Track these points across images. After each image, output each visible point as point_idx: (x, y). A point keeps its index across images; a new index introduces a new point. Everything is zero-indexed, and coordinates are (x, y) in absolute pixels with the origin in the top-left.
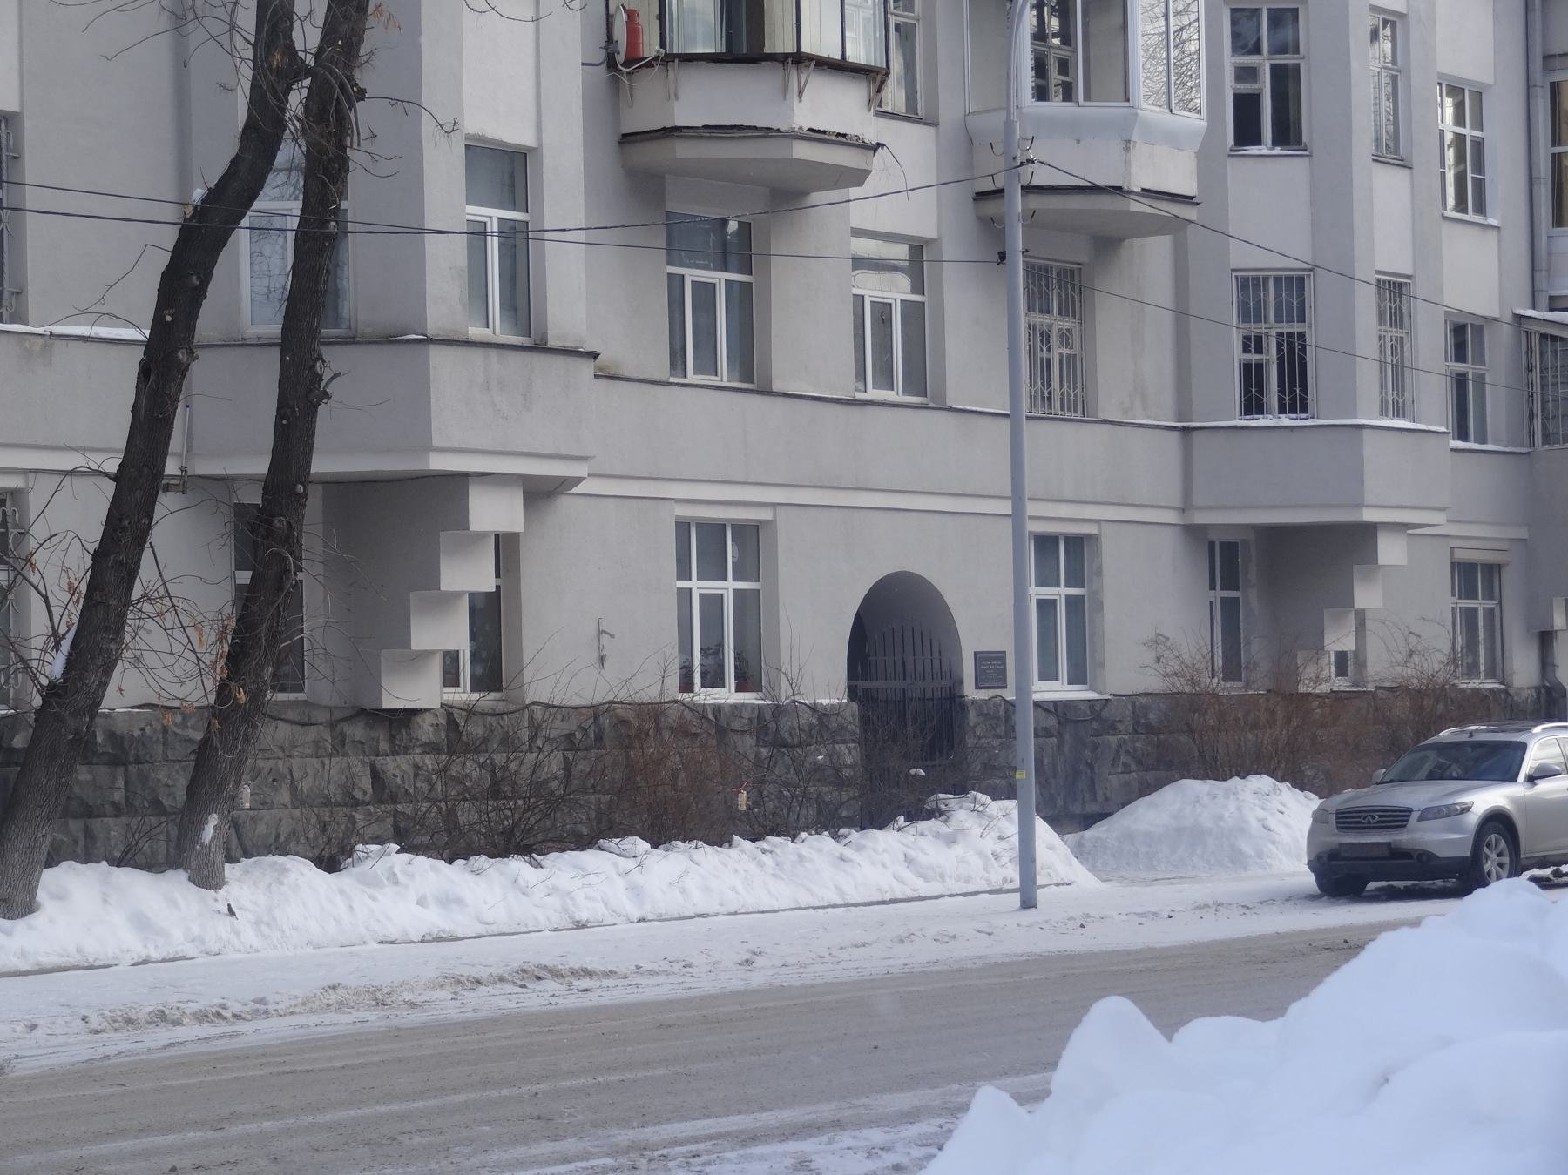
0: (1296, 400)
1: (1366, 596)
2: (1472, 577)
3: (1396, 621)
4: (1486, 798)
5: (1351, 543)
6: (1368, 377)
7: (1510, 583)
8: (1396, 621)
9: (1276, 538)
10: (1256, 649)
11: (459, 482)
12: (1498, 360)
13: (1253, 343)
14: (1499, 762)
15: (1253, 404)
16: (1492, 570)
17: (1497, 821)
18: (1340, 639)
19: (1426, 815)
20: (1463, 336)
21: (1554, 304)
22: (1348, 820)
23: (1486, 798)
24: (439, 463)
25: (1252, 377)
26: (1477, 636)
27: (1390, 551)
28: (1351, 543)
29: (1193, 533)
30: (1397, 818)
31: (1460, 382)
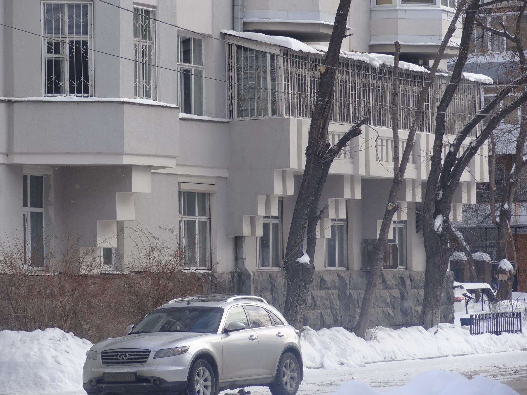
0: (81, 85)
1: (124, 213)
2: (192, 201)
3: (142, 229)
4: (197, 344)
5: (113, 178)
6: (127, 71)
7: (216, 206)
8: (142, 229)
9: (67, 174)
10: (53, 246)
11: (128, 169)
12: (210, 62)
13: (54, 47)
14: (204, 321)
15: (53, 86)
16: (205, 197)
17: (204, 359)
18: (107, 240)
19: (160, 354)
20: (188, 46)
21: (246, 27)
22: (109, 357)
23: (197, 344)
24: (127, 160)
25: (53, 69)
26: (193, 238)
27: (140, 184)
28: (113, 178)
29: (14, 169)
30: (141, 356)
31: (186, 75)
